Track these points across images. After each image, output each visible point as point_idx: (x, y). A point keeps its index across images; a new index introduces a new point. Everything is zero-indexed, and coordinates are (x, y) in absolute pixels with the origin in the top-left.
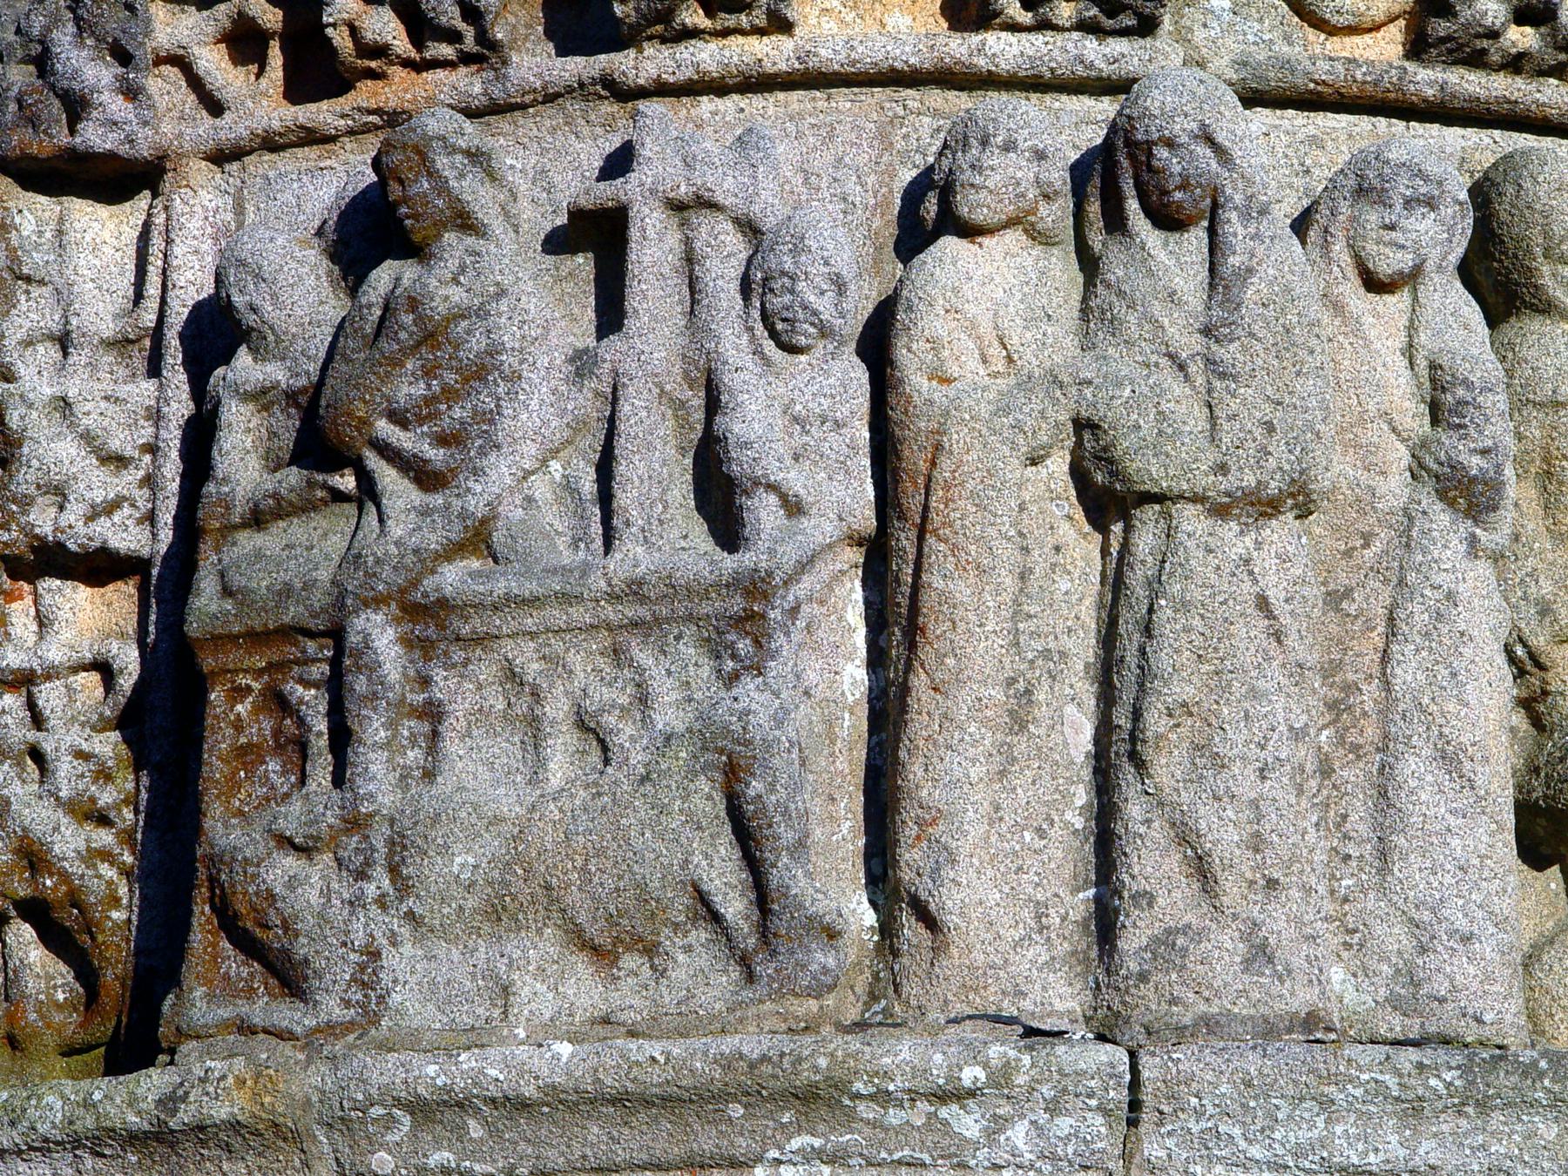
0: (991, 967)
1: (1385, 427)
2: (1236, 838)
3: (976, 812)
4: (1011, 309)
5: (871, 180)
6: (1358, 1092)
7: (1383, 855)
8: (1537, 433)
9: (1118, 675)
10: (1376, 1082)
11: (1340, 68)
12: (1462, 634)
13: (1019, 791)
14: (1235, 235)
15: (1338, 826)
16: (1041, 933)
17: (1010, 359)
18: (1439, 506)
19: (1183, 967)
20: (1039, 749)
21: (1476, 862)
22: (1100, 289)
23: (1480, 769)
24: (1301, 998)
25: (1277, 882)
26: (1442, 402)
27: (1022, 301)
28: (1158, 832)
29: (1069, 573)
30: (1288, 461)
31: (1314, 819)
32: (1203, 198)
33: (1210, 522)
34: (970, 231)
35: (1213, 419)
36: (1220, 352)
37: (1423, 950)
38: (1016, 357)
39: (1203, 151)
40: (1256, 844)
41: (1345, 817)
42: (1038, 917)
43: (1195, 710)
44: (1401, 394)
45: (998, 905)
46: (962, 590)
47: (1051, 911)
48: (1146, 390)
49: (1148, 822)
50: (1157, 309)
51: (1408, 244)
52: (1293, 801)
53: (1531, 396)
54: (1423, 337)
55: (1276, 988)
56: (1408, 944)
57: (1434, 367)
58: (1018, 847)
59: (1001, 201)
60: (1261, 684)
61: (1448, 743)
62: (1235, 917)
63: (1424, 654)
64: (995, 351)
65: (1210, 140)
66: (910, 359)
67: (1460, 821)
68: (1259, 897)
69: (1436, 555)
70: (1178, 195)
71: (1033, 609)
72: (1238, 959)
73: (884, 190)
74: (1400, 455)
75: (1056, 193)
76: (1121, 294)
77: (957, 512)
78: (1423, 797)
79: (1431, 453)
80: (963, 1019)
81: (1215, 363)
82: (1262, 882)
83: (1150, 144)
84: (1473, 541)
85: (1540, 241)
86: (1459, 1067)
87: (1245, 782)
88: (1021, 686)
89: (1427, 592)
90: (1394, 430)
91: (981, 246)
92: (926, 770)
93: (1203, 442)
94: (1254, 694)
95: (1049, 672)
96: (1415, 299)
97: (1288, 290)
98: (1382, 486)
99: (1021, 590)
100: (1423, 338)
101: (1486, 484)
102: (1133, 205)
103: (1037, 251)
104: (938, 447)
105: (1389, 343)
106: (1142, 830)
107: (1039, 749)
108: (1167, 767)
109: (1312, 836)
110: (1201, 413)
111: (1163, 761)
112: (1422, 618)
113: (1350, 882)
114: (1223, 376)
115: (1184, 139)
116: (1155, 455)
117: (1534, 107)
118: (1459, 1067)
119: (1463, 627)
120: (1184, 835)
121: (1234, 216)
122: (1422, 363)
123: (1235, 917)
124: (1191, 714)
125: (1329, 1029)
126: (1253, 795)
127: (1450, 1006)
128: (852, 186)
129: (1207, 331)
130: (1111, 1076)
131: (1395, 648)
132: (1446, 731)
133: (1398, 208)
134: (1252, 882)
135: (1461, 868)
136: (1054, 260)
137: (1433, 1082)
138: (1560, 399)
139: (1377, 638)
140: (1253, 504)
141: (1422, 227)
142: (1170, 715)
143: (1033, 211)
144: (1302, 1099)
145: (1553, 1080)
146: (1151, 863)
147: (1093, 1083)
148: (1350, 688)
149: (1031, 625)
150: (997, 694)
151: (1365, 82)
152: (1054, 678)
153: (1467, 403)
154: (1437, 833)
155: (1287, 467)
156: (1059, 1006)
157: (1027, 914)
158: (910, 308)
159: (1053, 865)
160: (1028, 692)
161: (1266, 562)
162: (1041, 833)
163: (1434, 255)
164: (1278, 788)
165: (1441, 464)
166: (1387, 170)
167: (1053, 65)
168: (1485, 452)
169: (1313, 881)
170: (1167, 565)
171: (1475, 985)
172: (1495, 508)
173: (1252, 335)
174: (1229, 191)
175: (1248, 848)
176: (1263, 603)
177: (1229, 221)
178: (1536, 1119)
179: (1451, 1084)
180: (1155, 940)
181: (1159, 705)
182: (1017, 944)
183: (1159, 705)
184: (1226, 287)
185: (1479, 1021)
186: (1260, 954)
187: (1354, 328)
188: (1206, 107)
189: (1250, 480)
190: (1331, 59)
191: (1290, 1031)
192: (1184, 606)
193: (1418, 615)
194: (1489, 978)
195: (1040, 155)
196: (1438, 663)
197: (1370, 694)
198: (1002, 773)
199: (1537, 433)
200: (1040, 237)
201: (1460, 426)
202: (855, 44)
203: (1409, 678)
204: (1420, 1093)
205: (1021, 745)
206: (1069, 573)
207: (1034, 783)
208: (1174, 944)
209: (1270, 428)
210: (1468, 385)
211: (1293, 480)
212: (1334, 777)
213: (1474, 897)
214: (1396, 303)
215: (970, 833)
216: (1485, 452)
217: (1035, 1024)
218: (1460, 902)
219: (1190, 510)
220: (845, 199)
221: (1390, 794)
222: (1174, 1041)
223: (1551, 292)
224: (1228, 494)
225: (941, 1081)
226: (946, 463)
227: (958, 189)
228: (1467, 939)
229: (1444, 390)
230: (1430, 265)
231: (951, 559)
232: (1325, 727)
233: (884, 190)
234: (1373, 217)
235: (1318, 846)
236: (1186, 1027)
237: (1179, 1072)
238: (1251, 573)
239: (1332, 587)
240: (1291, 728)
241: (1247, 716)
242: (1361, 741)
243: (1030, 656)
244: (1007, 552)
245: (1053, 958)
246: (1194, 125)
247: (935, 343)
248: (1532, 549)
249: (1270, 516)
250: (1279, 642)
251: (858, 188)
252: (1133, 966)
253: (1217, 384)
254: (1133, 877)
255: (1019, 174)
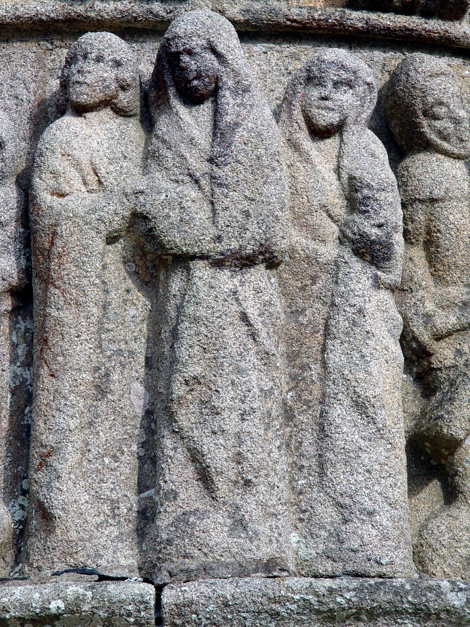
0: (81, 540)
1: (325, 215)
2: (225, 456)
3: (73, 447)
4: (101, 153)
5: (32, 86)
6: (294, 607)
7: (321, 465)
8: (422, 218)
9: (159, 363)
10: (304, 600)
11: (305, 11)
12: (368, 332)
13: (101, 434)
14: (228, 104)
15: (297, 449)
16: (114, 518)
17: (100, 182)
18: (354, 259)
19: (192, 534)
20: (114, 408)
21: (377, 467)
22: (154, 140)
23: (379, 412)
24: (265, 552)
25: (250, 481)
26: (355, 196)
27: (108, 148)
28: (181, 455)
29: (135, 305)
30: (258, 233)
31: (278, 444)
32: (210, 83)
33: (212, 270)
34: (81, 110)
35: (214, 211)
36: (219, 172)
37: (346, 521)
38: (103, 180)
39: (209, 56)
40: (239, 459)
41: (301, 443)
42: (113, 510)
43: (202, 381)
44: (332, 193)
45: (87, 502)
46: (67, 315)
47: (121, 505)
48: (174, 195)
49: (175, 449)
50: (183, 149)
51: (336, 108)
52: (262, 432)
53: (417, 196)
54: (346, 161)
55: (248, 545)
56: (337, 518)
57: (352, 178)
58: (100, 467)
59: (94, 91)
60: (243, 364)
61: (359, 397)
62: (224, 503)
63: (346, 345)
64: (91, 178)
65: (214, 51)
66: (42, 185)
67: (367, 443)
68: (240, 491)
69: (352, 287)
70: (195, 83)
71: (111, 326)
72: (226, 529)
73: (40, 91)
74: (333, 229)
75: (128, 85)
76: (164, 141)
77: (65, 270)
78: (345, 429)
79: (349, 228)
80: (62, 573)
81: (215, 178)
82: (242, 482)
83: (179, 53)
84: (376, 279)
85: (421, 106)
86: (354, 590)
87: (231, 422)
88: (103, 371)
89: (348, 309)
90: (330, 216)
91: (85, 118)
92: (45, 423)
93: (208, 224)
94: (239, 371)
95: (121, 363)
96: (342, 141)
97: (259, 135)
98: (322, 249)
99: (103, 316)
100: (346, 162)
101: (381, 244)
102: (172, 91)
103: (120, 120)
104: (55, 233)
105: (327, 166)
106: (172, 453)
107: (114, 408)
108: (186, 417)
109: (275, 455)
110: (207, 207)
111: (183, 412)
112: (344, 324)
113: (303, 482)
114: (220, 185)
115: (198, 50)
116: (179, 232)
117: (423, 32)
118: (354, 590)
119: (368, 328)
120: (196, 457)
121: (227, 93)
122: (345, 176)
123: (224, 503)
124: (200, 383)
125: (282, 570)
126: (237, 430)
127: (360, 555)
128: (21, 90)
129: (211, 160)
130: (141, 603)
131: (329, 342)
132: (358, 390)
133: (330, 85)
134: (236, 482)
135: (368, 471)
136: (131, 125)
137: (339, 599)
138: (435, 197)
139: (319, 336)
140: (237, 259)
141: (344, 98)
142: (187, 384)
143: (115, 97)
144: (259, 613)
145: (413, 597)
146: (177, 472)
147: (130, 608)
148: (304, 367)
149: (110, 335)
150: (88, 377)
151: (320, 20)
152: (124, 366)
153: (369, 198)
154: (353, 451)
155: (257, 237)
156: (123, 562)
157: (106, 508)
158: (41, 155)
159: (123, 478)
160: (107, 375)
161: (246, 292)
162: (115, 458)
163: (352, 115)
164: (254, 426)
165: (355, 234)
166: (323, 66)
167: (134, 15)
168: (380, 226)
169: (276, 480)
170: (187, 296)
171: (376, 542)
172: (389, 259)
173: (238, 161)
174: (225, 79)
175: (233, 462)
176: (244, 317)
177: (224, 96)
178: (406, 621)
179: (350, 600)
180: (178, 519)
181: (180, 379)
182: (99, 526)
183: (180, 379)
184: (222, 134)
185: (379, 563)
186: (239, 524)
187: (307, 159)
188: (211, 31)
189: (235, 245)
190: (300, 7)
191: (256, 571)
192: (196, 320)
193: (341, 323)
194: (386, 538)
195: (118, 64)
196: (353, 349)
197: (315, 370)
198: (91, 424)
199: (422, 218)
200: (121, 112)
201: (366, 212)
202: (18, 6)
203: (337, 360)
204: (331, 606)
205: (102, 407)
206: (135, 305)
207: (110, 428)
208: (188, 521)
209: (247, 215)
210: (369, 186)
211: (261, 244)
212: (295, 420)
213: (376, 488)
214: (332, 143)
215: (68, 461)
216: (380, 226)
217: (107, 574)
218: (367, 491)
219: (201, 264)
220: (17, 98)
221: (326, 429)
222: (185, 579)
223: (428, 136)
224: (222, 254)
225: (38, 611)
226: (59, 242)
227: (71, 85)
228: (371, 514)
229: (357, 191)
230: (349, 120)
231: (62, 298)
232: (290, 390)
233: (40, 91)
234: (315, 93)
235: (283, 462)
236: (192, 571)
237: (184, 599)
238: (237, 300)
239: (294, 308)
240: (262, 390)
241: (233, 383)
242: (311, 398)
243: (109, 353)
244: (94, 294)
245: (121, 534)
246: (204, 42)
247: (55, 174)
248: (420, 285)
249: (250, 266)
250: (254, 339)
251: (25, 90)
252: (164, 536)
253: (217, 190)
254: (165, 482)
255: (105, 75)
